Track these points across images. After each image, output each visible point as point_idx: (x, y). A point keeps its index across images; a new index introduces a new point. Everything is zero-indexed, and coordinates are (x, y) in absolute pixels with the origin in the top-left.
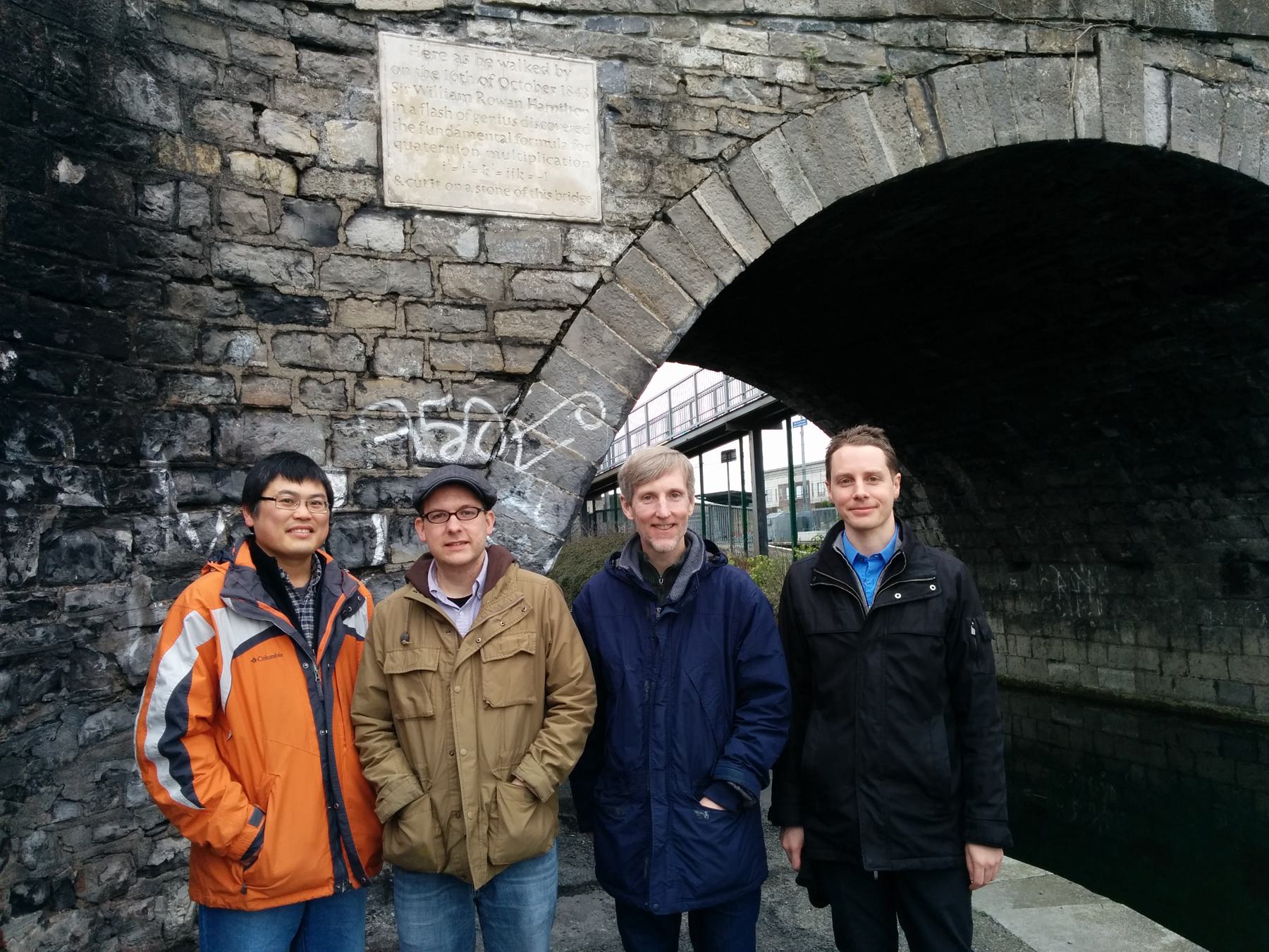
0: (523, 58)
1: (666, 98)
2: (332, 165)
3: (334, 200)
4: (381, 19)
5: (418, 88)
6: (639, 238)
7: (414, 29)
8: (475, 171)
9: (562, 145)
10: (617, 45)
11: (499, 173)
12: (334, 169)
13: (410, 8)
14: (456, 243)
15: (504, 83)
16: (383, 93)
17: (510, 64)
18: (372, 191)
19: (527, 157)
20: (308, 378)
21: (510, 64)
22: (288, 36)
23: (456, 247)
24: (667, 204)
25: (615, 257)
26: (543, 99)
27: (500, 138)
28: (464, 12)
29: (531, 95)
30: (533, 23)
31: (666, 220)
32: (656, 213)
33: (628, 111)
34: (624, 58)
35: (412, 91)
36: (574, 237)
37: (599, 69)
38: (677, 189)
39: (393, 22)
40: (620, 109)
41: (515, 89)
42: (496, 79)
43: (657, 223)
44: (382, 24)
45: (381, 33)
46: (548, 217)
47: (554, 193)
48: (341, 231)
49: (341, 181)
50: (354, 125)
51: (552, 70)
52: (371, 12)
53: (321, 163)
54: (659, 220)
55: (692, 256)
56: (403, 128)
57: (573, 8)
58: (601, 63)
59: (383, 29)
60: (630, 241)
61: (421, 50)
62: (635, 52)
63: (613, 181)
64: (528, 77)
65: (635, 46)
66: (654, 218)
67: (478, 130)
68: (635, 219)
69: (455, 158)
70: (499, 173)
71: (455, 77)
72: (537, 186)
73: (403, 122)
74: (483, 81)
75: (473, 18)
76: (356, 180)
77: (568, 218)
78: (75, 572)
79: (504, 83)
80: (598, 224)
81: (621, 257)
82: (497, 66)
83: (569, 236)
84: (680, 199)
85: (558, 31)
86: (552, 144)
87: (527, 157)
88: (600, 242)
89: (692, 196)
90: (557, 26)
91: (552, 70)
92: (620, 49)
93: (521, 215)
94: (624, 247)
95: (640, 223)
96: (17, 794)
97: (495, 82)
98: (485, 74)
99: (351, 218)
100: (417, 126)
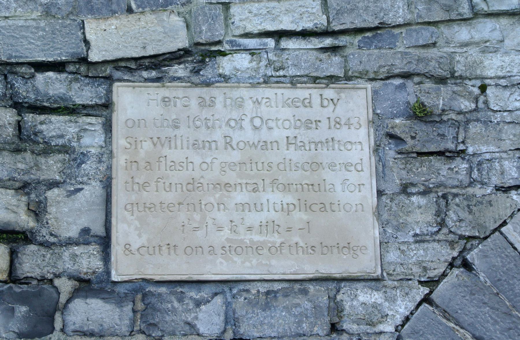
0: (279, 91)
1: (460, 118)
2: (52, 240)
3: (51, 281)
4: (117, 68)
5: (155, 140)
6: (431, 292)
7: (154, 74)
8: (220, 229)
9: (328, 187)
10: (397, 62)
11: (250, 229)
12: (54, 244)
13: (150, 52)
14: (196, 318)
15: (257, 122)
16: (115, 151)
17: (265, 100)
18: (97, 264)
19: (285, 206)
20: (262, 121)
21: (265, 100)
22: (10, 103)
23: (196, 322)
24: (468, 246)
25: (399, 320)
26: (304, 135)
27: (250, 188)
28: (214, 48)
29: (290, 133)
30: (295, 50)
31: (467, 266)
32: (454, 259)
33: (413, 138)
34: (406, 76)
35: (147, 145)
36: (345, 297)
37: (375, 92)
38: (481, 226)
39: (130, 70)
40: (403, 136)
41: (270, 128)
42: (247, 120)
43: (456, 271)
44: (117, 74)
45: (116, 84)
46: (311, 276)
47: (318, 249)
48: (58, 318)
49: (60, 257)
50: (80, 190)
51: (316, 101)
52: (105, 62)
53: (40, 239)
54: (459, 267)
55: (504, 309)
56: (136, 187)
57: (342, 27)
58: (378, 84)
59: (120, 80)
60: (418, 299)
61: (160, 98)
62: (421, 68)
63: (395, 223)
64: (286, 113)
65: (420, 60)
66: (451, 266)
67: (225, 179)
68: (425, 269)
69: (197, 217)
70: (250, 229)
71: (198, 123)
72: (296, 239)
73: (137, 180)
74: (233, 123)
75: (223, 54)
76: (78, 253)
77: (338, 276)
78: (37, 43)
79: (257, 122)
80: (377, 280)
81: (407, 319)
82: (249, 105)
83: (339, 297)
84: (486, 238)
85: (323, 56)
86: (316, 188)
87: (285, 206)
88: (379, 301)
89: (502, 233)
90: (324, 50)
91: (316, 101)
92: (400, 67)
93: (276, 277)
94: (412, 306)
95: (432, 274)
96: (278, 1)
97: (246, 124)
98: (235, 115)
99: (69, 301)
100: (153, 184)
